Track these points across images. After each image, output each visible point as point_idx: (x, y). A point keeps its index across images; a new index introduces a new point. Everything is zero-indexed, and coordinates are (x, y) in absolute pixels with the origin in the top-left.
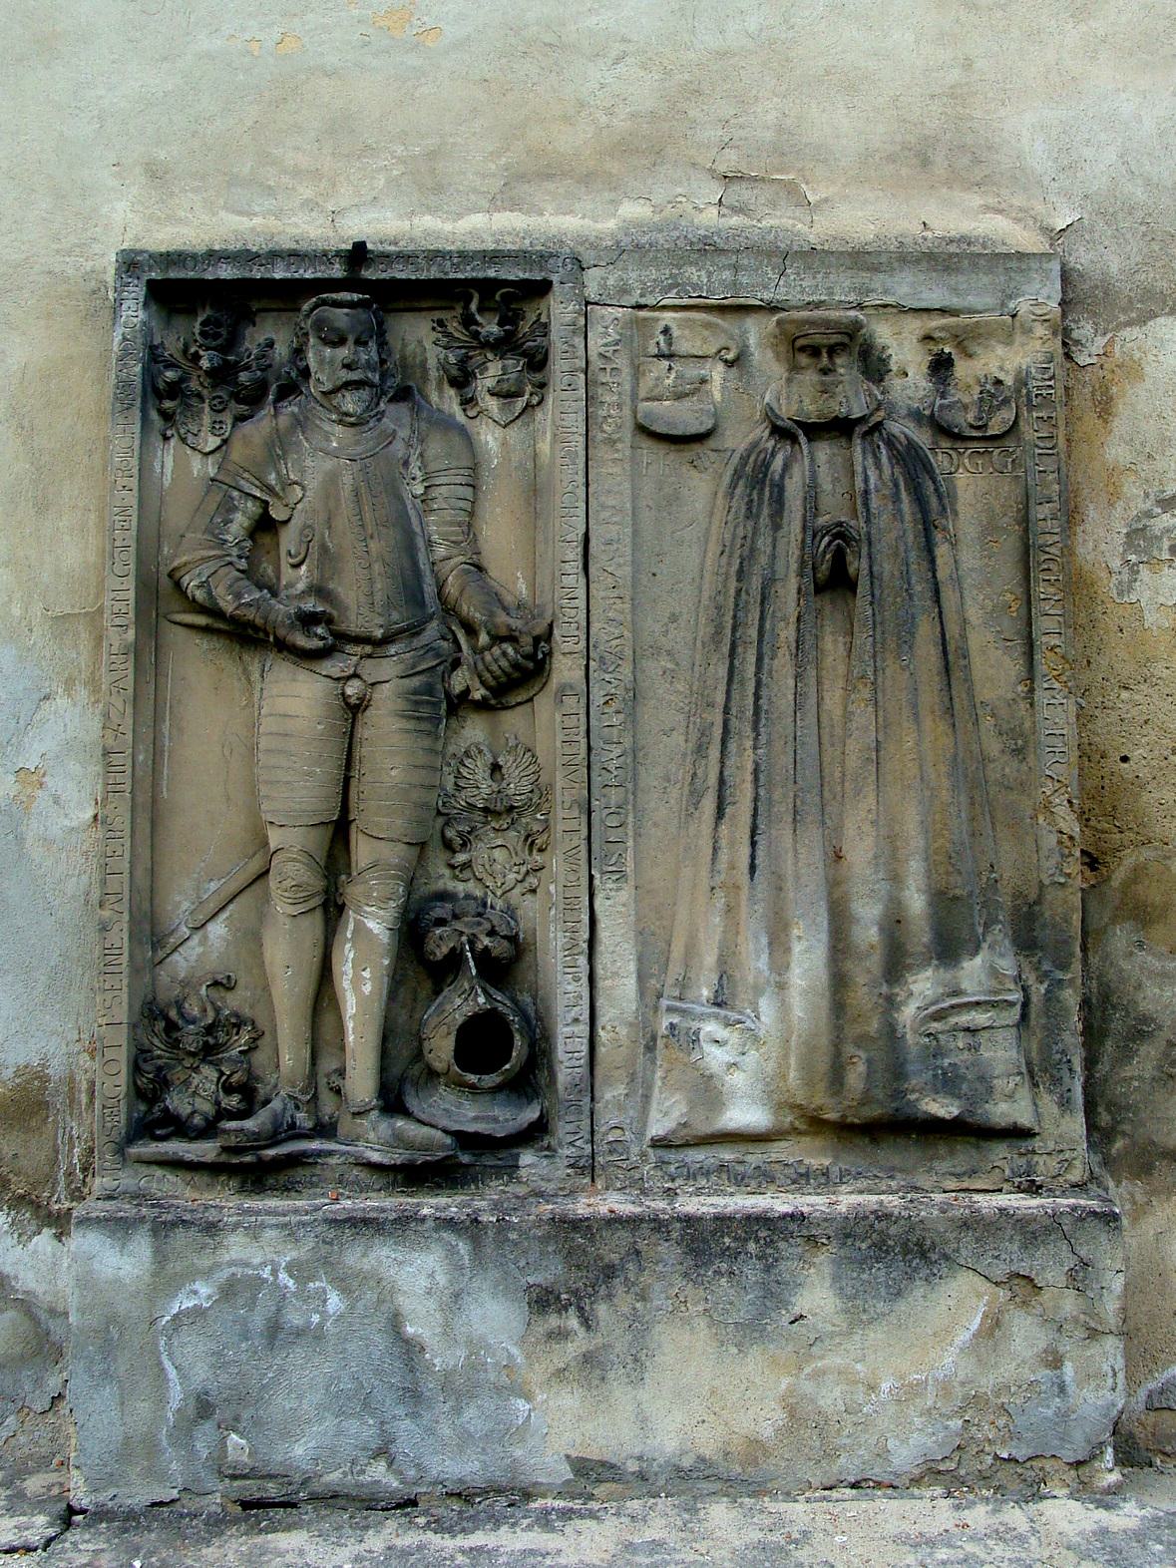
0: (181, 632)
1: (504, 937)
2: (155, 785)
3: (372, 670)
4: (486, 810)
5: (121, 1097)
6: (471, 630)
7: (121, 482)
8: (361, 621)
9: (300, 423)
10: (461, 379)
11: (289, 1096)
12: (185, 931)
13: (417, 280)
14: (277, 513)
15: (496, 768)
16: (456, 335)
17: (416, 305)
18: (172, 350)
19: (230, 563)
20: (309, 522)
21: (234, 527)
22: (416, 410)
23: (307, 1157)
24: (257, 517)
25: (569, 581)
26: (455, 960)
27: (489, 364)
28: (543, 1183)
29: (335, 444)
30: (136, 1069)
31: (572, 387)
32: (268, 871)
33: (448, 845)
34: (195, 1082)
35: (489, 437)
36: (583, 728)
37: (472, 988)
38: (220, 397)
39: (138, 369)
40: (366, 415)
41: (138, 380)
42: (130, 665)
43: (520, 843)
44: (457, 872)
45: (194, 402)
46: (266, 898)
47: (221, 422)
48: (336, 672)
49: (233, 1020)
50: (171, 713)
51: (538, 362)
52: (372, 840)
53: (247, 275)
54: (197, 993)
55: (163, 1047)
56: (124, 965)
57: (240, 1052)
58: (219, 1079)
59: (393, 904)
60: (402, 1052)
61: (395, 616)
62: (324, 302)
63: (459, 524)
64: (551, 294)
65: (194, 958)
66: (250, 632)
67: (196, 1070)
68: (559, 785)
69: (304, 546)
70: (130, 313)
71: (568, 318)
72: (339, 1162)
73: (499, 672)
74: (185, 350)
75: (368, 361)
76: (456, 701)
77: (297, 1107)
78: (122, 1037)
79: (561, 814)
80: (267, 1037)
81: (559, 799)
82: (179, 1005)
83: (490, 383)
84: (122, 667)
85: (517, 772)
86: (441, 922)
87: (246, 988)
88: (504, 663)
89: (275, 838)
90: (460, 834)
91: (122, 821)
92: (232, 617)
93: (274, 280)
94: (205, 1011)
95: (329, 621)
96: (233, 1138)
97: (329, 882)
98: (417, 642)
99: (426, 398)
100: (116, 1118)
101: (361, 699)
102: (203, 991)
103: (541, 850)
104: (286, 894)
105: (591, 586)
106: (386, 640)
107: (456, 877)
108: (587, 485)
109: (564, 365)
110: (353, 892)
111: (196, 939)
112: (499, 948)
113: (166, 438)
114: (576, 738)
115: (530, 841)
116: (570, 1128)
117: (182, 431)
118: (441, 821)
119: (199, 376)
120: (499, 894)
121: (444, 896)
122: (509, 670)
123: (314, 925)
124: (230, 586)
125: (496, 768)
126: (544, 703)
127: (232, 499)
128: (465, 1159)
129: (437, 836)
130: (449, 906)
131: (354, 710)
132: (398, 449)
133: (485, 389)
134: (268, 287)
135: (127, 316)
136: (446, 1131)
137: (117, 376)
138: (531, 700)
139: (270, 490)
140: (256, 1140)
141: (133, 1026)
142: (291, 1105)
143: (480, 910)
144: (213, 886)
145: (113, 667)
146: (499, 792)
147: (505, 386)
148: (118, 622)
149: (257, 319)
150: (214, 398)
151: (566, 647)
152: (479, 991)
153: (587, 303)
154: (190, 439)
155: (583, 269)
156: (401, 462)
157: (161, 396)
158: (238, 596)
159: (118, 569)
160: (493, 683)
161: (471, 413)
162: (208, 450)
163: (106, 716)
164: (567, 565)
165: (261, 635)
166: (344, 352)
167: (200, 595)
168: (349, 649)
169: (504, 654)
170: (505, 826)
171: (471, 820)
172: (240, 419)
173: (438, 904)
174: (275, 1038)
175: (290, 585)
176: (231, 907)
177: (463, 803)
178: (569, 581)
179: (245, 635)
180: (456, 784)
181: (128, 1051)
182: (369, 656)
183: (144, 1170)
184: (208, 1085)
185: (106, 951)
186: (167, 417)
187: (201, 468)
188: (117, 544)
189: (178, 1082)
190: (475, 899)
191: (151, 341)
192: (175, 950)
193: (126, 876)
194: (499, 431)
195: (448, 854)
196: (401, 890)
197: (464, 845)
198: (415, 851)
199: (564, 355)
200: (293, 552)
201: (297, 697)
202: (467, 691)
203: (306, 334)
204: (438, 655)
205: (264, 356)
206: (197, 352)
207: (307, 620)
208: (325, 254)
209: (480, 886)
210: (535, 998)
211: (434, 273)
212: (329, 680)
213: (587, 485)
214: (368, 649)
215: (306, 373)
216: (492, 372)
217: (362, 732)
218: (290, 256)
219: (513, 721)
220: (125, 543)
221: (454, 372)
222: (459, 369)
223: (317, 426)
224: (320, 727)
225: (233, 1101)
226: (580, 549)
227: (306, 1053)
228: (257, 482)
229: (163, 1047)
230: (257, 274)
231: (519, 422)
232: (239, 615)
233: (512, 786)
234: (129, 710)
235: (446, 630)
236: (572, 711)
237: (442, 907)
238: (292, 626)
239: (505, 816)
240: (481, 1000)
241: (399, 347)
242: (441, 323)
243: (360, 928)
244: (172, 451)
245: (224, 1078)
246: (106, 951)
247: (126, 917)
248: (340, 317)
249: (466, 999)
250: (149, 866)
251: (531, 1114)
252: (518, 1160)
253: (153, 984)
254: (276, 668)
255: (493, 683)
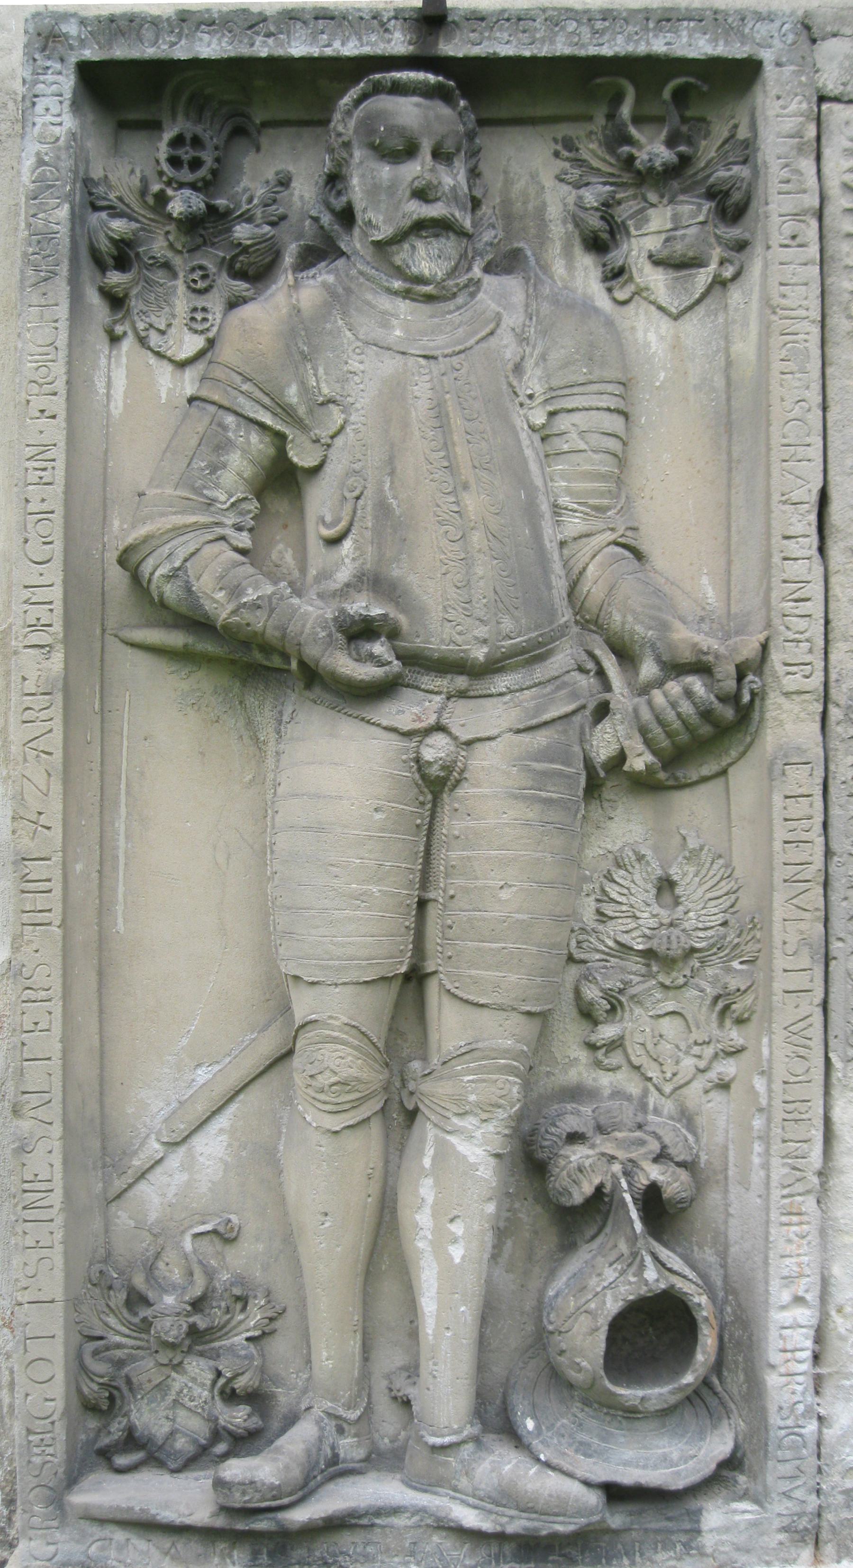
0: (143, 662)
1: (680, 1164)
2: (104, 909)
3: (466, 720)
4: (649, 954)
5: (55, 1417)
6: (625, 655)
7: (37, 403)
8: (448, 631)
9: (339, 299)
10: (601, 240)
11: (329, 1415)
12: (155, 1147)
13: (534, 59)
14: (302, 456)
15: (666, 886)
16: (596, 163)
17: (529, 112)
18: (123, 191)
19: (223, 538)
20: (357, 466)
21: (228, 478)
22: (533, 285)
23: (360, 1517)
24: (266, 463)
25: (797, 569)
26: (600, 1203)
27: (651, 212)
28: (735, 1555)
29: (398, 333)
30: (78, 1367)
31: (798, 240)
32: (290, 1053)
33: (587, 1014)
34: (176, 1386)
35: (650, 334)
36: (819, 819)
37: (635, 1255)
38: (201, 268)
39: (63, 212)
40: (451, 283)
41: (63, 231)
42: (56, 712)
43: (704, 1009)
44: (600, 1054)
45: (159, 276)
46: (289, 1085)
47: (204, 310)
48: (406, 723)
49: (237, 1291)
50: (128, 793)
51: (732, 207)
52: (469, 1008)
53: (245, 51)
54: (179, 1246)
55: (127, 1331)
56: (58, 1206)
57: (248, 1339)
58: (214, 1382)
59: (502, 1114)
60: (512, 1336)
61: (507, 625)
62: (377, 89)
63: (603, 477)
64: (758, 89)
65: (173, 1190)
66: (258, 656)
67: (178, 1367)
68: (778, 914)
69: (348, 507)
70: (49, 118)
71: (789, 125)
72: (409, 1523)
73: (677, 725)
74: (143, 192)
75: (454, 189)
76: (602, 774)
77: (340, 1431)
78: (54, 1321)
79: (780, 962)
80: (291, 1317)
81: (778, 938)
82: (150, 1270)
83: (652, 243)
84: (43, 715)
85: (700, 892)
86: (574, 1138)
87: (257, 1240)
88: (686, 708)
89: (304, 1004)
90: (607, 995)
91: (48, 975)
92: (226, 627)
93: (292, 60)
94: (191, 1274)
95: (394, 634)
96: (237, 1495)
97: (391, 1071)
98: (540, 672)
99: (545, 268)
100: (50, 1450)
101: (448, 768)
102: (188, 1244)
103: (740, 1021)
104: (322, 1097)
105: (833, 580)
106: (493, 667)
107: (598, 1064)
108: (825, 409)
109: (788, 204)
110: (435, 1091)
111: (175, 1160)
112: (673, 1182)
113: (114, 339)
114: (804, 836)
115: (724, 1007)
116: (787, 1469)
117: (141, 326)
118: (574, 971)
119: (168, 233)
120: (668, 1088)
121: (577, 1093)
122: (695, 719)
123: (366, 1149)
124: (222, 577)
125: (666, 886)
126: (745, 778)
127: (225, 428)
128: (616, 1520)
129: (569, 996)
130: (587, 1110)
131: (435, 786)
132: (506, 346)
133: (644, 254)
134: (280, 69)
135: (44, 124)
136: (587, 1483)
137: (29, 225)
138: (724, 772)
139: (286, 412)
140: (275, 1498)
141: (74, 1303)
142: (331, 1426)
143: (640, 1118)
144: (203, 1075)
145: (28, 715)
146: (671, 925)
147: (679, 248)
148: (34, 639)
149: (264, 141)
150: (193, 270)
151: (791, 683)
152: (648, 1259)
153: (822, 99)
154: (154, 339)
155: (814, 41)
156: (510, 366)
157: (110, 269)
158: (235, 591)
159: (36, 550)
160: (665, 743)
161: (621, 295)
162: (183, 356)
163: (19, 798)
164: (791, 543)
165: (276, 662)
166: (413, 170)
167: (171, 592)
168: (428, 681)
169: (688, 693)
170: (681, 981)
171: (623, 970)
172: (233, 304)
173: (569, 1107)
174: (304, 1317)
175: (325, 575)
176: (233, 1108)
177: (611, 943)
178: (797, 569)
179: (250, 663)
180: (599, 912)
181: (66, 1344)
182: (462, 695)
183: (96, 1531)
184: (197, 1391)
185: (27, 1186)
186: (116, 301)
187: (170, 386)
188: (31, 508)
189: (148, 1386)
190: (629, 1098)
191: (87, 170)
192: (142, 1176)
193: (56, 1063)
194: (665, 325)
195: (585, 1025)
196: (515, 1089)
197: (613, 1010)
198: (534, 1026)
199: (785, 187)
200: (328, 519)
201: (340, 768)
202: (621, 757)
203: (347, 145)
204: (574, 695)
205: (275, 201)
206: (162, 192)
207: (359, 632)
208: (376, 16)
209: (636, 1076)
210: (723, 1255)
211: (561, 48)
212: (393, 736)
213: (825, 409)
214: (461, 682)
215: (347, 217)
216: (654, 227)
217: (451, 824)
218: (316, 18)
219: (694, 810)
220: (45, 507)
221: (595, 222)
222: (602, 218)
223: (368, 303)
224: (378, 816)
225: (238, 1417)
226: (813, 517)
227: (354, 1344)
228: (267, 401)
229: (127, 1331)
230: (262, 49)
231: (701, 310)
232: (238, 625)
233: (691, 914)
234: (57, 787)
235: (585, 657)
236: (800, 791)
237: (578, 1113)
238: (330, 641)
239: (680, 964)
240: (651, 1274)
241: (499, 185)
242: (569, 144)
243: (444, 1153)
244: (124, 360)
245: (222, 1381)
246: (27, 1186)
247: (57, 1130)
248: (407, 111)
249: (623, 1273)
250: (96, 1043)
251: (719, 1445)
252: (698, 1521)
253: (107, 1231)
254: (301, 717)
255: (665, 743)
